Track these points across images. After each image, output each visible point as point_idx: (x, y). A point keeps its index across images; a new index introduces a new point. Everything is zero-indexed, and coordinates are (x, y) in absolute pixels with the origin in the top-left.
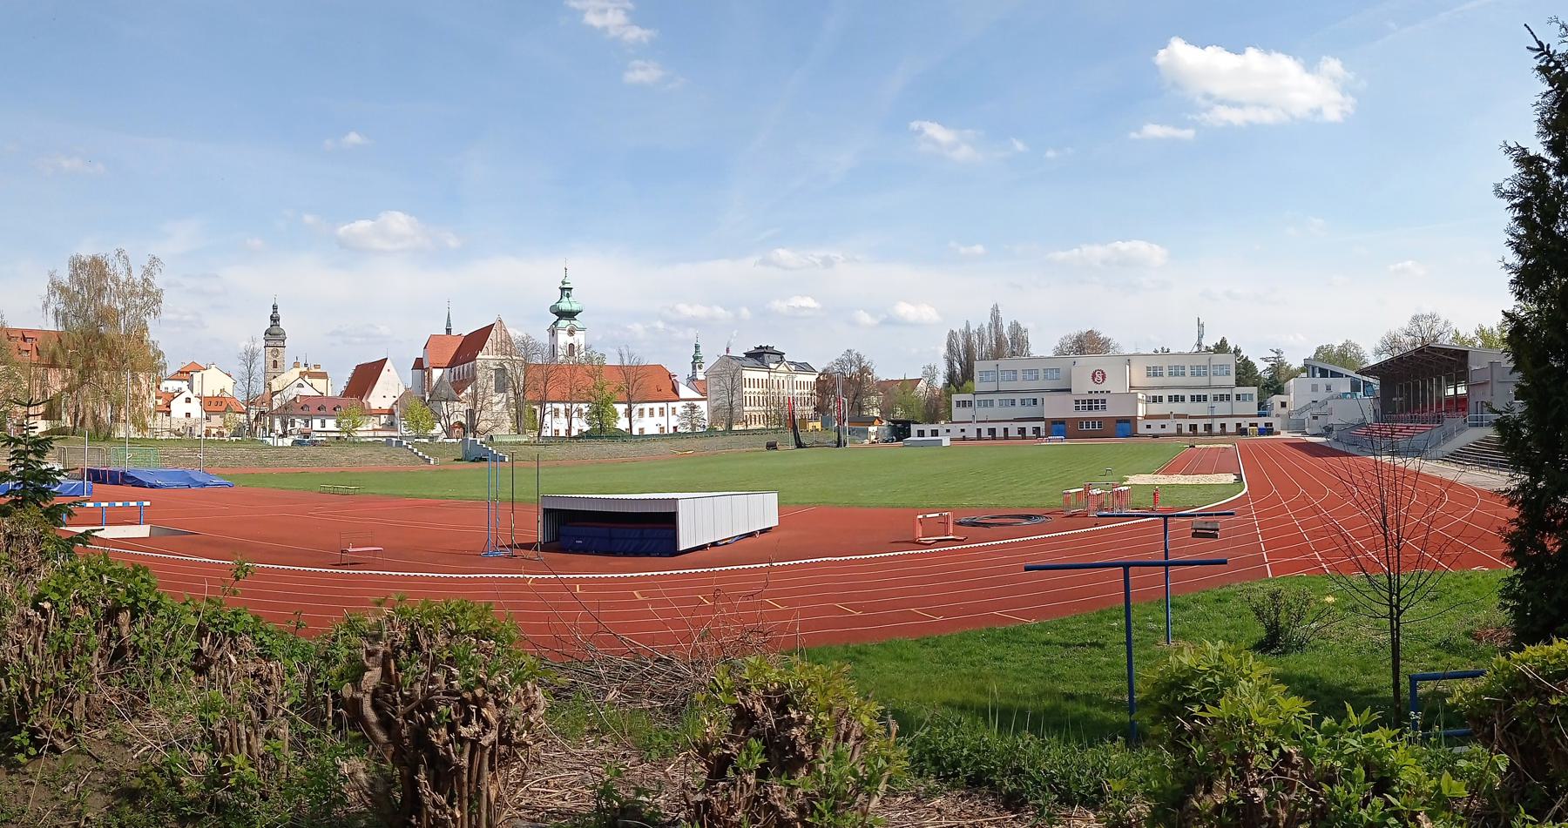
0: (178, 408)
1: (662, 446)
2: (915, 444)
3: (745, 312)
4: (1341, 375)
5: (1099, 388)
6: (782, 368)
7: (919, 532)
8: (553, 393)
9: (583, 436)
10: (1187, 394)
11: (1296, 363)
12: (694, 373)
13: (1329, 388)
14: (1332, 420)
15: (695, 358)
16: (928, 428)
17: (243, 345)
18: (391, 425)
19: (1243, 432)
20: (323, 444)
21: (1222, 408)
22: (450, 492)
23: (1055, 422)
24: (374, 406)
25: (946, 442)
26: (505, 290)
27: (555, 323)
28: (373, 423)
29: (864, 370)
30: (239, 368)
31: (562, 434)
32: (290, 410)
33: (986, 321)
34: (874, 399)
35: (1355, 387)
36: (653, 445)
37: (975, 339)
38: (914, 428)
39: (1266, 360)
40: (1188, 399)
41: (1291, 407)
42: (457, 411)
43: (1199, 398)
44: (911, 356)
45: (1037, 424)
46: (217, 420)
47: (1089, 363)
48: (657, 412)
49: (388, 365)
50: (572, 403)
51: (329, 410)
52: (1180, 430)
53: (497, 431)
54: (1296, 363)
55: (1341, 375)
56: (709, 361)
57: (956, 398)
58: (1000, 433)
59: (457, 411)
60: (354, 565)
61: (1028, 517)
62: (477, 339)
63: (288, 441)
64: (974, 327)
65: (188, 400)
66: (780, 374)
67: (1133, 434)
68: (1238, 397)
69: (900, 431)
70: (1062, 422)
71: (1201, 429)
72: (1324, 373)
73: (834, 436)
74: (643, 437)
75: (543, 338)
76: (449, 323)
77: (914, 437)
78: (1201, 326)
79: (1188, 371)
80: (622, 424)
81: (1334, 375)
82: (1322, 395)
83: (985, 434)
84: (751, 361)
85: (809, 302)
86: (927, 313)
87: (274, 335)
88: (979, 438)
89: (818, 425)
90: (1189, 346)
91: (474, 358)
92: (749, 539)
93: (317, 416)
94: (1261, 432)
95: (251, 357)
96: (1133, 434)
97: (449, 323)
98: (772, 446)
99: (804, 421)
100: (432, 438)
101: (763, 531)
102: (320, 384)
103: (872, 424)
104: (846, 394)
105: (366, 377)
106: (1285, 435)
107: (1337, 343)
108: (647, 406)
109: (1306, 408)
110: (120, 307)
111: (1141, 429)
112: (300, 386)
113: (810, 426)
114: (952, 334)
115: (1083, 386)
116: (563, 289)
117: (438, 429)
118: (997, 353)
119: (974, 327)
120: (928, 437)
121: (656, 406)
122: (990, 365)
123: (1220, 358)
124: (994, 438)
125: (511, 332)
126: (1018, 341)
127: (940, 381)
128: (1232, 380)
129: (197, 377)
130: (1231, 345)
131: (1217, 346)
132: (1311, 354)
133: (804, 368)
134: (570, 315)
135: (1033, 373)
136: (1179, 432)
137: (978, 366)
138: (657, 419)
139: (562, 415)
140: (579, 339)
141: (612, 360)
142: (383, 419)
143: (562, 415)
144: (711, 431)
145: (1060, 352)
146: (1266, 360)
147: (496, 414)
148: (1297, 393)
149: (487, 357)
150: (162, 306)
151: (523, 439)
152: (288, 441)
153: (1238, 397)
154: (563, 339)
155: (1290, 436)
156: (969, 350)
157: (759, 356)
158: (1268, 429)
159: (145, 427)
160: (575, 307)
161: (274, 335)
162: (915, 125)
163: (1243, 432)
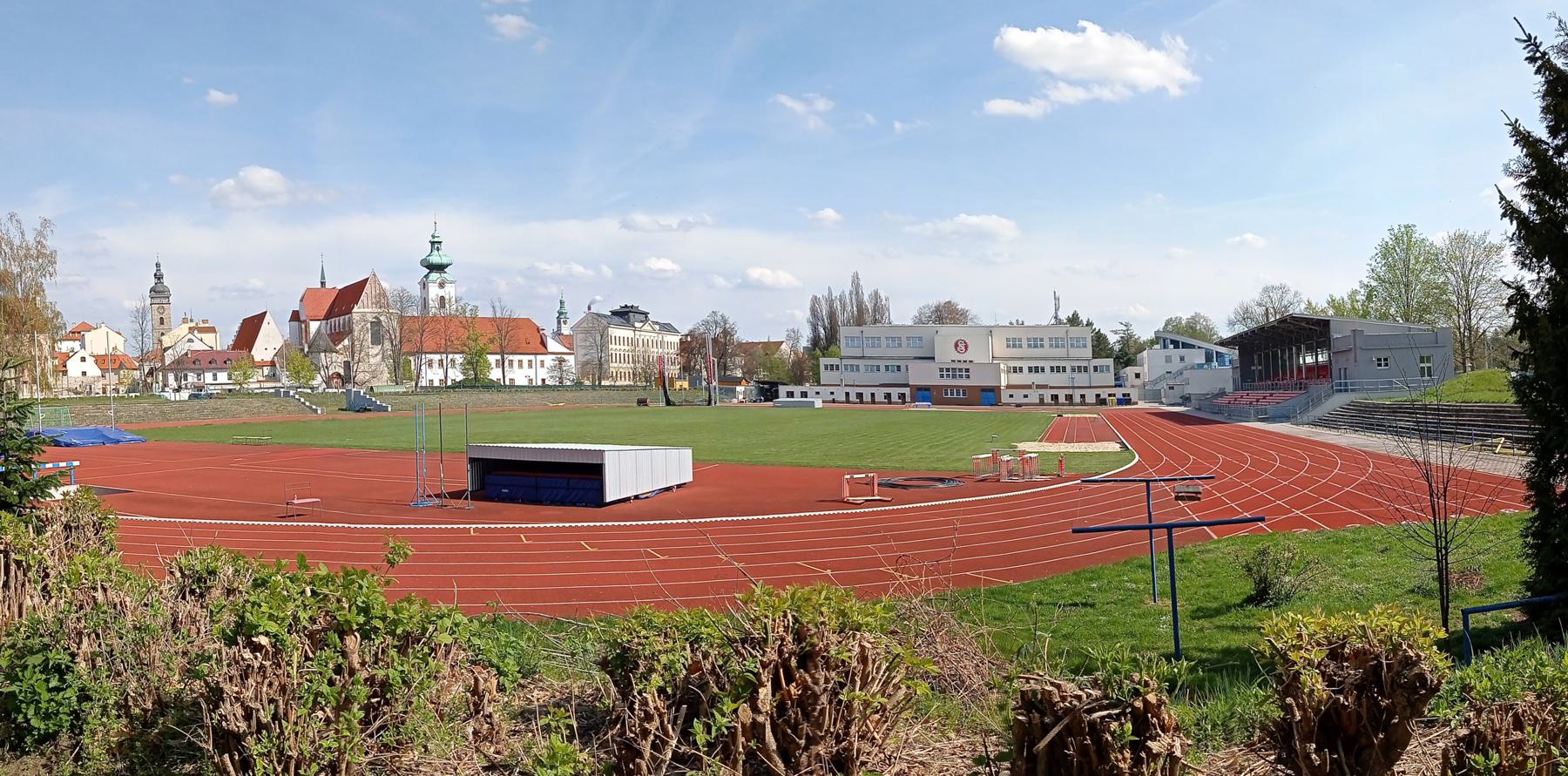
0: (74, 367)
1: (534, 398)
2: (785, 405)
3: (606, 271)
4: (1193, 347)
5: (962, 357)
6: (647, 327)
7: (846, 493)
8: (429, 343)
9: (457, 386)
10: (1047, 365)
11: (1144, 334)
12: (559, 328)
13: (1182, 359)
14: (1188, 390)
15: (560, 313)
16: (797, 390)
17: (132, 304)
18: (273, 377)
19: (1102, 402)
20: (219, 397)
21: (1081, 379)
22: (347, 441)
23: (920, 388)
24: (257, 358)
25: (818, 404)
26: (380, 242)
27: (426, 276)
28: (259, 375)
29: (726, 332)
30: (129, 326)
31: (436, 383)
32: (183, 365)
33: (848, 288)
34: (738, 360)
35: (1209, 358)
36: (525, 396)
37: (837, 304)
38: (783, 390)
39: (1115, 332)
40: (1047, 370)
41: (1145, 378)
42: (334, 362)
43: (1037, 370)
44: (777, 320)
45: (902, 390)
46: (112, 378)
47: (949, 332)
48: (525, 364)
49: (268, 318)
50: (447, 353)
51: (220, 363)
52: (1042, 400)
53: (374, 383)
54: (1144, 334)
55: (1193, 347)
56: (576, 315)
57: (823, 361)
58: (867, 398)
59: (334, 362)
60: (299, 516)
61: (942, 480)
62: (351, 294)
63: (185, 395)
64: (836, 294)
65: (83, 359)
66: (646, 334)
67: (996, 402)
68: (1096, 369)
69: (768, 392)
70: (927, 388)
71: (1062, 399)
72: (1176, 344)
73: (705, 395)
74: (513, 387)
75: (416, 291)
76: (323, 277)
77: (783, 398)
78: (1057, 299)
79: (1025, 343)
80: (495, 374)
81: (1185, 346)
82: (1176, 366)
83: (853, 398)
84: (617, 319)
85: (665, 264)
86: (784, 278)
87: (159, 292)
88: (848, 401)
89: (686, 385)
90: (1046, 319)
91: (350, 312)
92: (668, 494)
93: (209, 370)
94: (1120, 402)
95: (141, 315)
96: (996, 402)
97: (323, 277)
98: (642, 402)
99: (671, 380)
100: (312, 388)
101: (679, 486)
102: (209, 338)
103: (739, 383)
104: (711, 354)
105: (250, 329)
106: (1142, 405)
107: (1185, 316)
108: (516, 358)
109: (1161, 379)
110: (16, 270)
111: (1005, 398)
112: (190, 341)
113: (678, 385)
114: (815, 300)
115: (946, 355)
116: (433, 243)
117: (318, 381)
118: (859, 321)
119: (836, 294)
120: (797, 398)
121: (525, 358)
122: (855, 330)
123: (1075, 331)
124: (862, 402)
125: (384, 285)
126: (879, 312)
127: (804, 343)
128: (1088, 352)
129: (88, 336)
130: (1084, 318)
131: (1069, 320)
132: (1161, 326)
133: (667, 328)
134: (440, 268)
135: (895, 341)
136: (1042, 403)
137: (844, 332)
138: (526, 370)
139: (436, 365)
140: (450, 291)
141: (485, 312)
142: (266, 371)
143: (436, 365)
144: (578, 385)
145: (919, 321)
146: (1115, 332)
147: (374, 368)
148: (1151, 365)
149: (363, 311)
150: (57, 267)
151: (401, 389)
152: (185, 395)
153: (1096, 369)
154: (434, 292)
155: (1147, 406)
156: (832, 315)
157: (624, 315)
158: (1125, 400)
159: (48, 387)
160: (445, 261)
161: (159, 292)
162: (1083, 23)
163: (1102, 402)
